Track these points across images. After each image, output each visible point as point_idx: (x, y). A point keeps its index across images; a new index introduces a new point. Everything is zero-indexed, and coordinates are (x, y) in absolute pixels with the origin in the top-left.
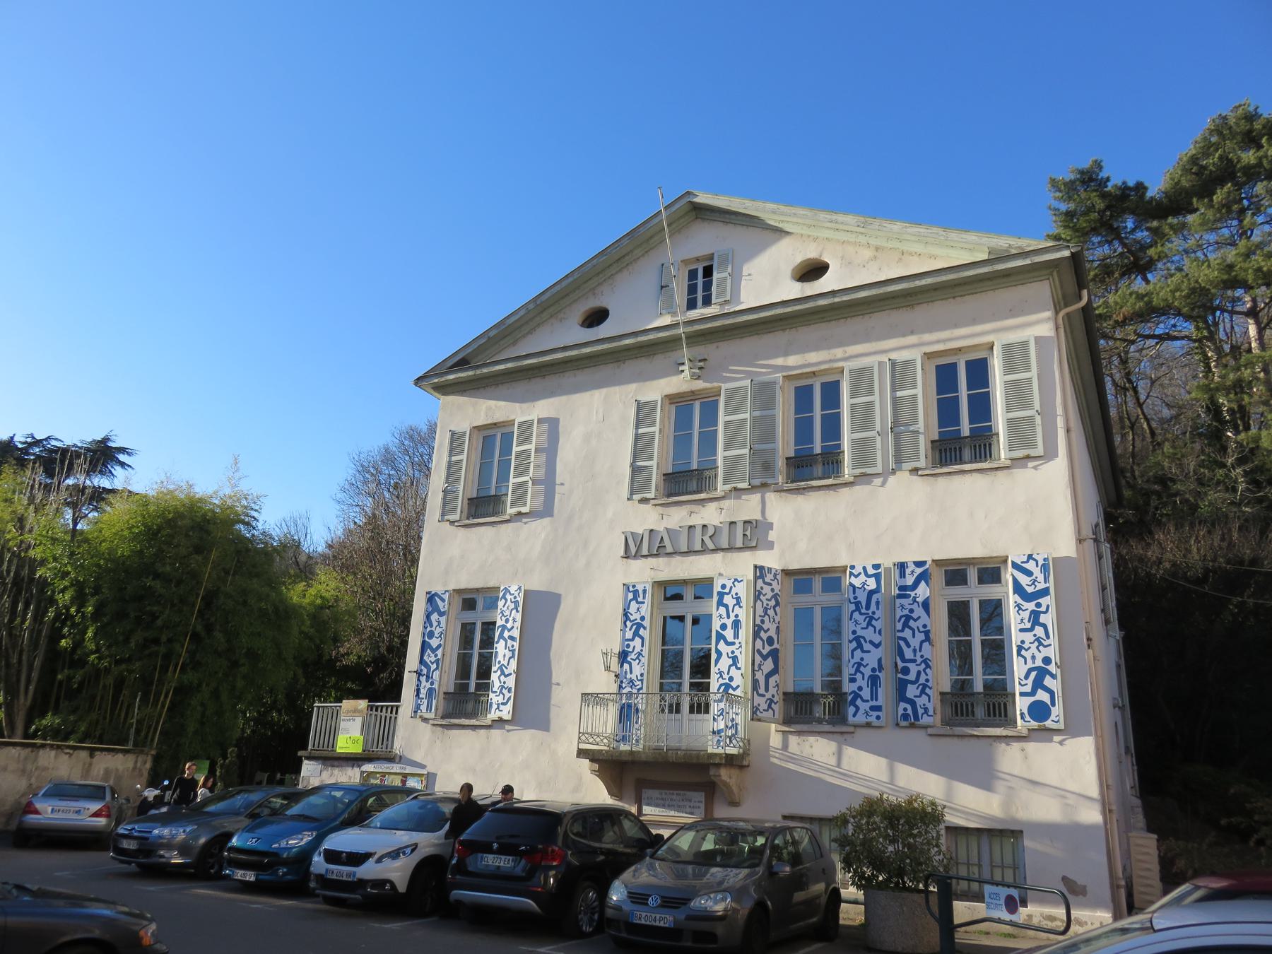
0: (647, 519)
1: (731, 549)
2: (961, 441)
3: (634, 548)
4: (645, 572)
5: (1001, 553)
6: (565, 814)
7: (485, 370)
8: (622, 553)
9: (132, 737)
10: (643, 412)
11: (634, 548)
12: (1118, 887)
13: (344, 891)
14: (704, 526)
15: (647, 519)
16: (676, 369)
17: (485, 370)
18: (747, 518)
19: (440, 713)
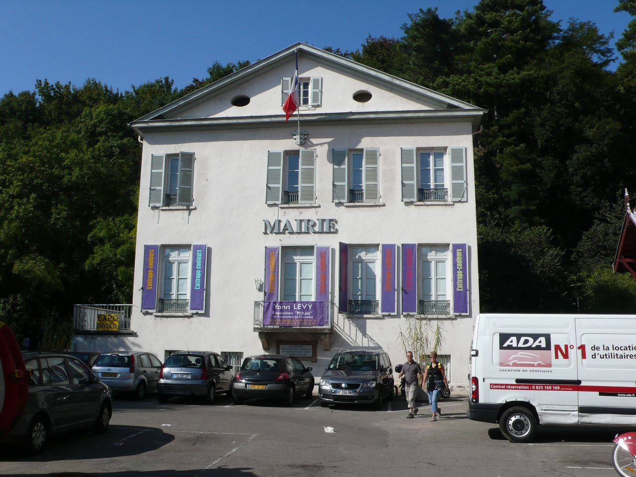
0: (273, 215)
1: (322, 232)
2: (425, 193)
3: (271, 228)
4: (276, 241)
5: (449, 243)
6: (344, 343)
7: (177, 124)
8: (264, 231)
9: (351, 377)
10: (272, 158)
11: (271, 228)
12: (149, 269)
13: (570, 386)
14: (309, 221)
15: (273, 215)
16: (291, 136)
17: (177, 124)
18: (331, 218)
19: (158, 310)
